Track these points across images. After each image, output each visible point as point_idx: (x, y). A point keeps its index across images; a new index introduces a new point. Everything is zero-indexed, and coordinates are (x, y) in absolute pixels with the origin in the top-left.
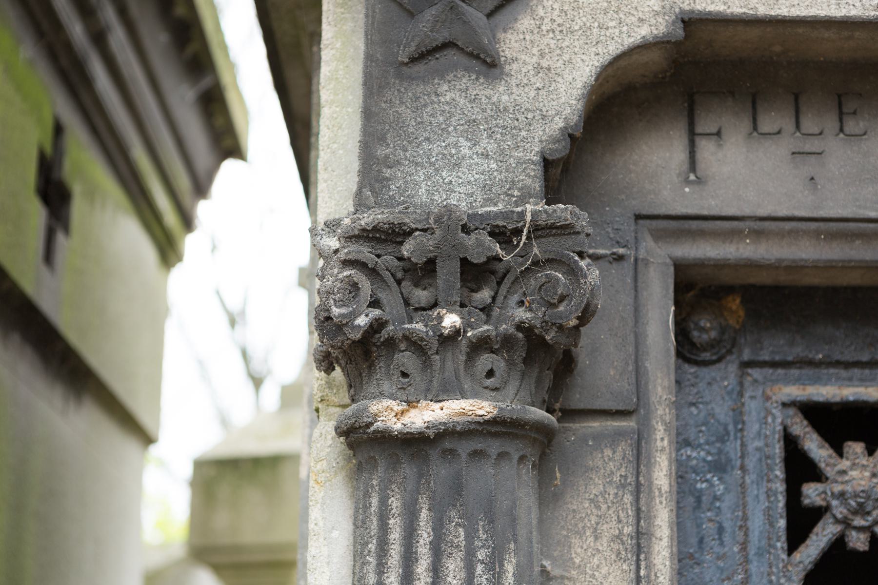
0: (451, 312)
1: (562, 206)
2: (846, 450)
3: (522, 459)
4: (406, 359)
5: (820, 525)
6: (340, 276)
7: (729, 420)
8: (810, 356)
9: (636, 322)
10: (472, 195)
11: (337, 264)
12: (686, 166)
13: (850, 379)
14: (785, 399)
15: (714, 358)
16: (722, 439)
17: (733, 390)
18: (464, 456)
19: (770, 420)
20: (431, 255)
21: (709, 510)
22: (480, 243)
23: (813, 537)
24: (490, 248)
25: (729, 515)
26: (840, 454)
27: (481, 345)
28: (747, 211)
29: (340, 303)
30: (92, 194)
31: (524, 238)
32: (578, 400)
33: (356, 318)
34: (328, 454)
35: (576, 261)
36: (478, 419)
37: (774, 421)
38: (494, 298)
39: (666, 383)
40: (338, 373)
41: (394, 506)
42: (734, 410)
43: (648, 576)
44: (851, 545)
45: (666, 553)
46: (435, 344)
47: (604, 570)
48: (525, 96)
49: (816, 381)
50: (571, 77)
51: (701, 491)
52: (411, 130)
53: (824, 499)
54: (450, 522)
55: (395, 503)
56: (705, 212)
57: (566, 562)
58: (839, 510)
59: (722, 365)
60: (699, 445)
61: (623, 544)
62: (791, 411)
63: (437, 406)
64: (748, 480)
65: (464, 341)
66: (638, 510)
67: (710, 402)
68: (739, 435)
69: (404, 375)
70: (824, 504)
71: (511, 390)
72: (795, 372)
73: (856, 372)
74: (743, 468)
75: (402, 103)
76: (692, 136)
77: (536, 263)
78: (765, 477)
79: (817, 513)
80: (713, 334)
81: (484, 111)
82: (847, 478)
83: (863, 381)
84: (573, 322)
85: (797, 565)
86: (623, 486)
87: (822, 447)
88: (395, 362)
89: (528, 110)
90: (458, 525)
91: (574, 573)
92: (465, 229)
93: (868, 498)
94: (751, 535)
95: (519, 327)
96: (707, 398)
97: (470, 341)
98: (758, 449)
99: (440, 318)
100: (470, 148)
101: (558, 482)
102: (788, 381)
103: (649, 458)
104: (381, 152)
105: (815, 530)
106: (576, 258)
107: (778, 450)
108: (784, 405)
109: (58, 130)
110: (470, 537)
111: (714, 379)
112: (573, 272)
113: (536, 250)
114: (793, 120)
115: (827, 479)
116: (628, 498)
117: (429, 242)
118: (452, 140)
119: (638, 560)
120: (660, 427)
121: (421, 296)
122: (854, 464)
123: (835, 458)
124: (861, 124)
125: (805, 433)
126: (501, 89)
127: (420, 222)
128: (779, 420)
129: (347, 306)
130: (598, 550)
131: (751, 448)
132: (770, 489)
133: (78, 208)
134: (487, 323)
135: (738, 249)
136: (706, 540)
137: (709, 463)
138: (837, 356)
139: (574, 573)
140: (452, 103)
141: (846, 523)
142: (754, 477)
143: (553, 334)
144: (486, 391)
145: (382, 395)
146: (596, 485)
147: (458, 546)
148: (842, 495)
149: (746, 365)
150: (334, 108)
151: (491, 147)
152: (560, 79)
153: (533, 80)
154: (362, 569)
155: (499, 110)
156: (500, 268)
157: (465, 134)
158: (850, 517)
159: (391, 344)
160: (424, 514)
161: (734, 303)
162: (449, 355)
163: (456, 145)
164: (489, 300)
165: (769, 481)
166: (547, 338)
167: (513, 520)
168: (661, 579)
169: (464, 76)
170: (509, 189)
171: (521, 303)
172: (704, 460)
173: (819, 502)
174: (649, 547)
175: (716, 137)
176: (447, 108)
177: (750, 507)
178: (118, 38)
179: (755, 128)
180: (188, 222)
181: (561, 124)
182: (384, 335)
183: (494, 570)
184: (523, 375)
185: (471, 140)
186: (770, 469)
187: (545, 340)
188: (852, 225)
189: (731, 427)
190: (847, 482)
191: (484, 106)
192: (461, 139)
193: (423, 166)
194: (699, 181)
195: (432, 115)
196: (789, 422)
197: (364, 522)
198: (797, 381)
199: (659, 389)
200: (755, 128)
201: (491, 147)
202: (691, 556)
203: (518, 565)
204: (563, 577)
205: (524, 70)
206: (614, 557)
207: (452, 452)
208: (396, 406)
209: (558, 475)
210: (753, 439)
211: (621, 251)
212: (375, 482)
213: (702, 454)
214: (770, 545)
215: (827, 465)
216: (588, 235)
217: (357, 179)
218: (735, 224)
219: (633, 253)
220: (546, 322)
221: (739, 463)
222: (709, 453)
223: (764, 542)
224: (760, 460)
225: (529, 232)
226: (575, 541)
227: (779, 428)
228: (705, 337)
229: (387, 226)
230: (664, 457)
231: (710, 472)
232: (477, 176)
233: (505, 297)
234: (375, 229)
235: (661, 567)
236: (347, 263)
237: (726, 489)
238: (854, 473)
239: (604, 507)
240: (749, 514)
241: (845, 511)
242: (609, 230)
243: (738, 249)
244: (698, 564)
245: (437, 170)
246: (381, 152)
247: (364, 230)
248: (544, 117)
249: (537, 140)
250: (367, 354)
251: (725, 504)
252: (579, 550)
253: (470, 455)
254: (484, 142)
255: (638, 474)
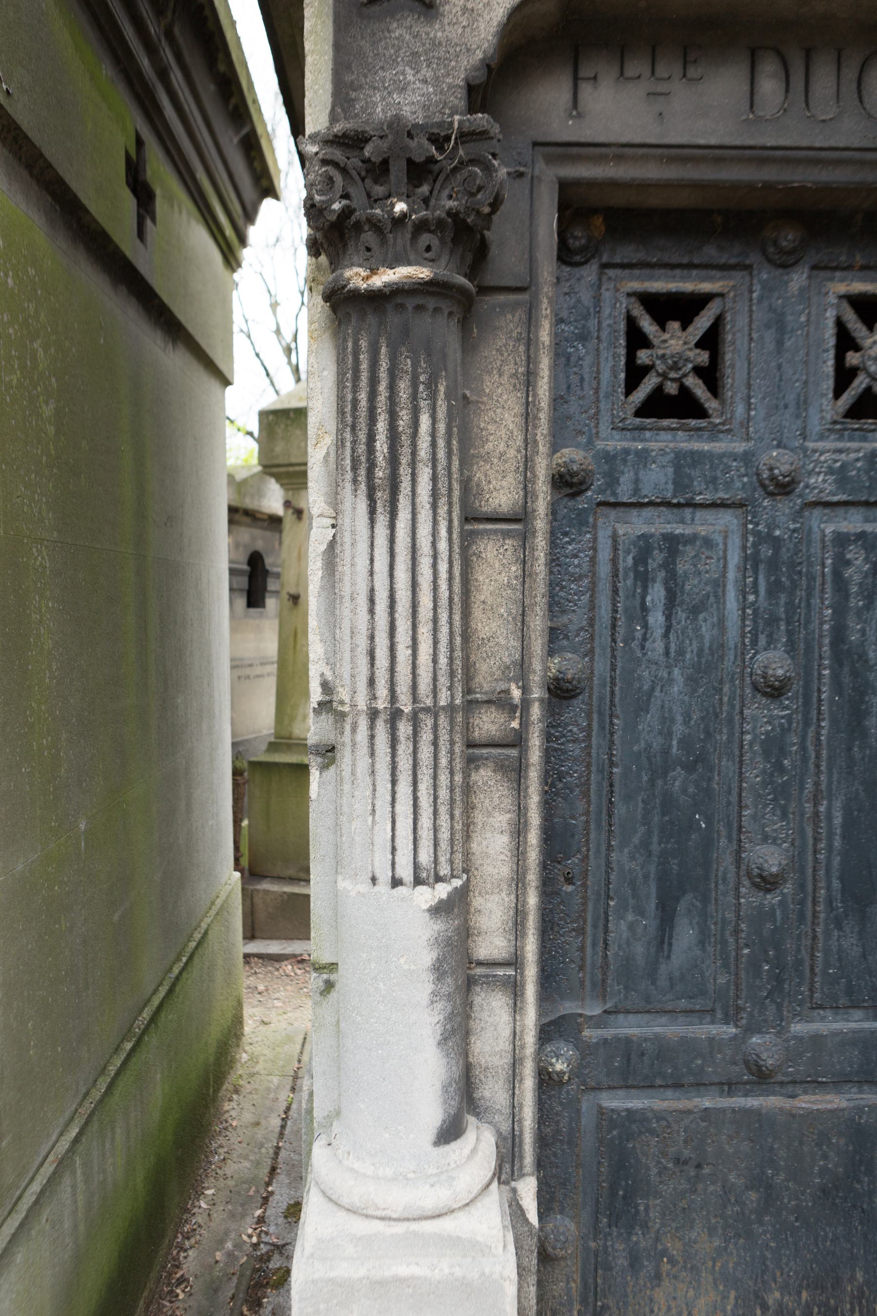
0: (401, 201)
1: (480, 115)
2: (667, 327)
3: (450, 314)
4: (369, 237)
5: (647, 377)
6: (320, 172)
7: (591, 305)
8: (649, 259)
9: (531, 224)
10: (415, 112)
11: (318, 163)
12: (570, 104)
13: (674, 277)
14: (629, 290)
15: (583, 260)
16: (586, 317)
17: (594, 284)
18: (410, 309)
19: (618, 305)
20: (386, 156)
21: (575, 366)
22: (420, 146)
23: (642, 385)
24: (427, 150)
25: (588, 370)
26: (664, 329)
27: (422, 227)
28: (612, 139)
29: (321, 192)
30: (170, 199)
31: (452, 142)
32: (490, 280)
33: (332, 204)
34: (319, 318)
35: (490, 160)
36: (420, 281)
37: (621, 306)
38: (431, 192)
39: (550, 269)
40: (323, 258)
41: (363, 345)
42: (594, 298)
43: (534, 401)
44: (667, 390)
45: (546, 387)
46: (389, 226)
47: (505, 397)
48: (454, 32)
49: (651, 278)
50: (489, 17)
51: (570, 353)
52: (370, 60)
53: (651, 360)
54: (401, 355)
55: (364, 344)
56: (583, 140)
57: (480, 392)
58: (660, 367)
59: (587, 266)
60: (570, 322)
61: (518, 379)
62: (633, 300)
63: (391, 272)
64: (601, 347)
65: (410, 223)
66: (529, 357)
67: (578, 292)
68: (597, 315)
69: (368, 249)
70: (651, 363)
71: (443, 261)
72: (637, 272)
73: (678, 272)
74: (598, 338)
75: (363, 38)
76: (576, 80)
77: (461, 163)
78: (613, 345)
79: (646, 370)
80: (583, 241)
81: (424, 45)
82: (667, 345)
83: (683, 279)
84: (487, 210)
85: (630, 404)
86: (519, 340)
87: (651, 325)
88: (361, 240)
89: (456, 44)
90: (407, 357)
91: (485, 399)
92: (410, 135)
93: (680, 358)
94: (602, 384)
95: (449, 213)
96: (577, 290)
97: (414, 223)
98: (609, 325)
99: (393, 205)
100: (414, 76)
101: (475, 335)
102: (632, 278)
103: (537, 321)
104: (349, 78)
105: (644, 381)
106: (490, 157)
107: (622, 326)
108: (629, 295)
109: (140, 143)
110: (415, 365)
111: (582, 276)
112: (488, 169)
113: (461, 152)
114: (650, 67)
115: (654, 346)
116: (522, 348)
117: (384, 145)
118: (400, 68)
119: (528, 391)
120: (545, 301)
121: (379, 190)
122: (672, 336)
123: (660, 333)
124: (699, 70)
125: (641, 315)
126: (437, 27)
127: (377, 130)
128: (624, 305)
129: (326, 195)
130: (501, 384)
131: (605, 324)
132: (615, 353)
133: (160, 205)
134: (426, 210)
135: (604, 171)
136: (572, 386)
137: (576, 334)
138: (666, 259)
139: (485, 399)
140: (400, 38)
141: (664, 376)
142: (605, 344)
143: (472, 217)
144: (426, 262)
145: (352, 265)
146: (501, 339)
147: (406, 372)
148: (663, 357)
149: (605, 266)
150: (314, 56)
151: (429, 74)
152: (480, 19)
153: (460, 19)
154: (343, 391)
155: (436, 44)
156: (436, 168)
157: (409, 63)
158: (667, 371)
159: (358, 227)
160: (383, 350)
161: (598, 221)
162: (399, 234)
163: (403, 73)
164: (428, 193)
165: (615, 347)
166: (469, 220)
167: (445, 356)
168: (542, 404)
169: (409, 16)
170: (443, 108)
171: (450, 197)
172: (573, 333)
173: (647, 362)
174: (535, 382)
175: (592, 81)
176: (396, 42)
177: (602, 365)
178: (177, 77)
179: (622, 74)
180: (243, 240)
181: (481, 56)
182: (353, 219)
183: (431, 388)
184: (452, 252)
185: (414, 69)
186: (617, 339)
187: (467, 223)
188: (687, 151)
189: (592, 310)
190: (667, 348)
191: (424, 41)
192: (407, 68)
193: (379, 90)
194: (579, 116)
195: (385, 48)
196: (631, 307)
197: (343, 359)
198: (638, 278)
199: (545, 273)
200: (622, 74)
201: (429, 74)
202: (562, 397)
203: (447, 386)
204: (477, 402)
205: (454, 11)
206: (511, 388)
207: (402, 306)
208: (363, 272)
209: (475, 330)
210: (606, 319)
211: (522, 169)
212: (350, 331)
213: (572, 328)
214: (614, 391)
215: (655, 337)
216: (499, 141)
217: (331, 100)
218: (603, 150)
219: (530, 171)
220: (468, 208)
221: (596, 335)
222: (576, 328)
223: (610, 389)
224: (610, 333)
225: (456, 139)
226: (486, 377)
227: (624, 311)
228: (577, 243)
229: (352, 133)
230: (547, 321)
231: (576, 340)
232: (419, 98)
233: (439, 191)
234: (345, 135)
235: (543, 396)
236: (325, 162)
237: (586, 352)
238: (672, 342)
239: (506, 354)
240: (601, 369)
241: (664, 368)
242: (514, 153)
243: (604, 171)
244: (566, 402)
245: (389, 93)
246: (349, 78)
247: (336, 136)
248: (468, 50)
249: (463, 69)
250: (342, 236)
251: (587, 362)
252: (488, 384)
253: (414, 308)
254: (424, 72)
255: (529, 332)
